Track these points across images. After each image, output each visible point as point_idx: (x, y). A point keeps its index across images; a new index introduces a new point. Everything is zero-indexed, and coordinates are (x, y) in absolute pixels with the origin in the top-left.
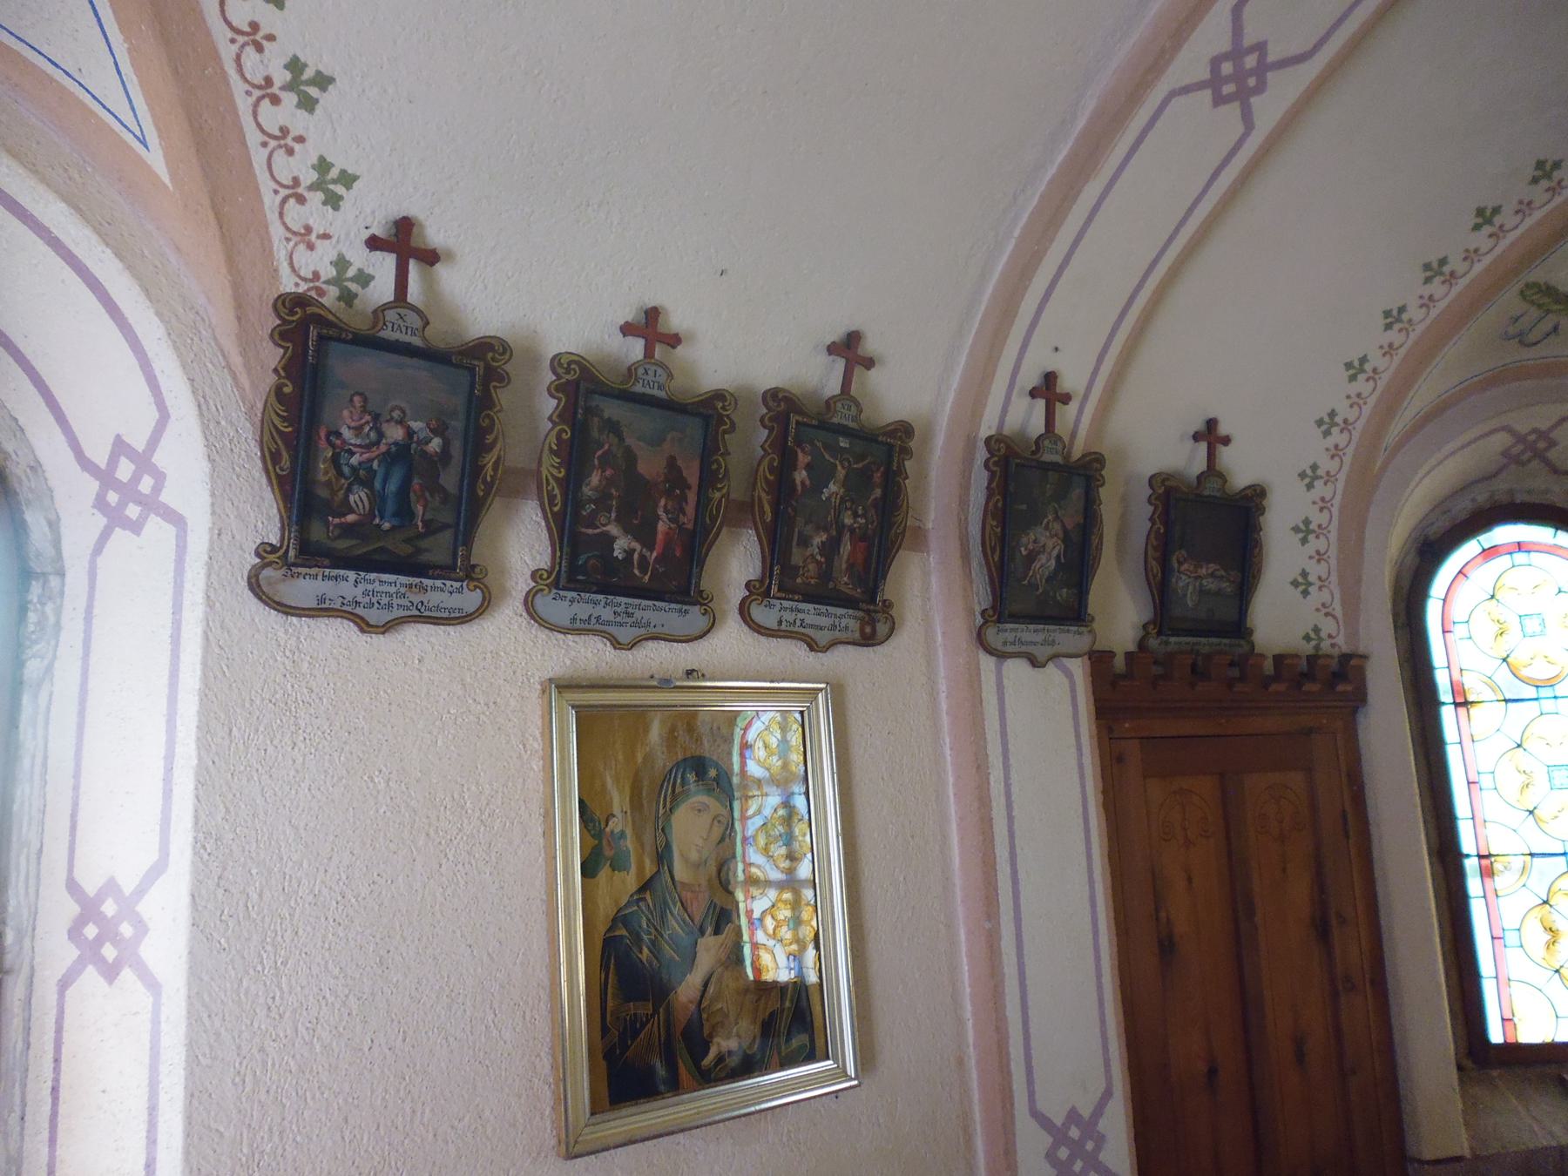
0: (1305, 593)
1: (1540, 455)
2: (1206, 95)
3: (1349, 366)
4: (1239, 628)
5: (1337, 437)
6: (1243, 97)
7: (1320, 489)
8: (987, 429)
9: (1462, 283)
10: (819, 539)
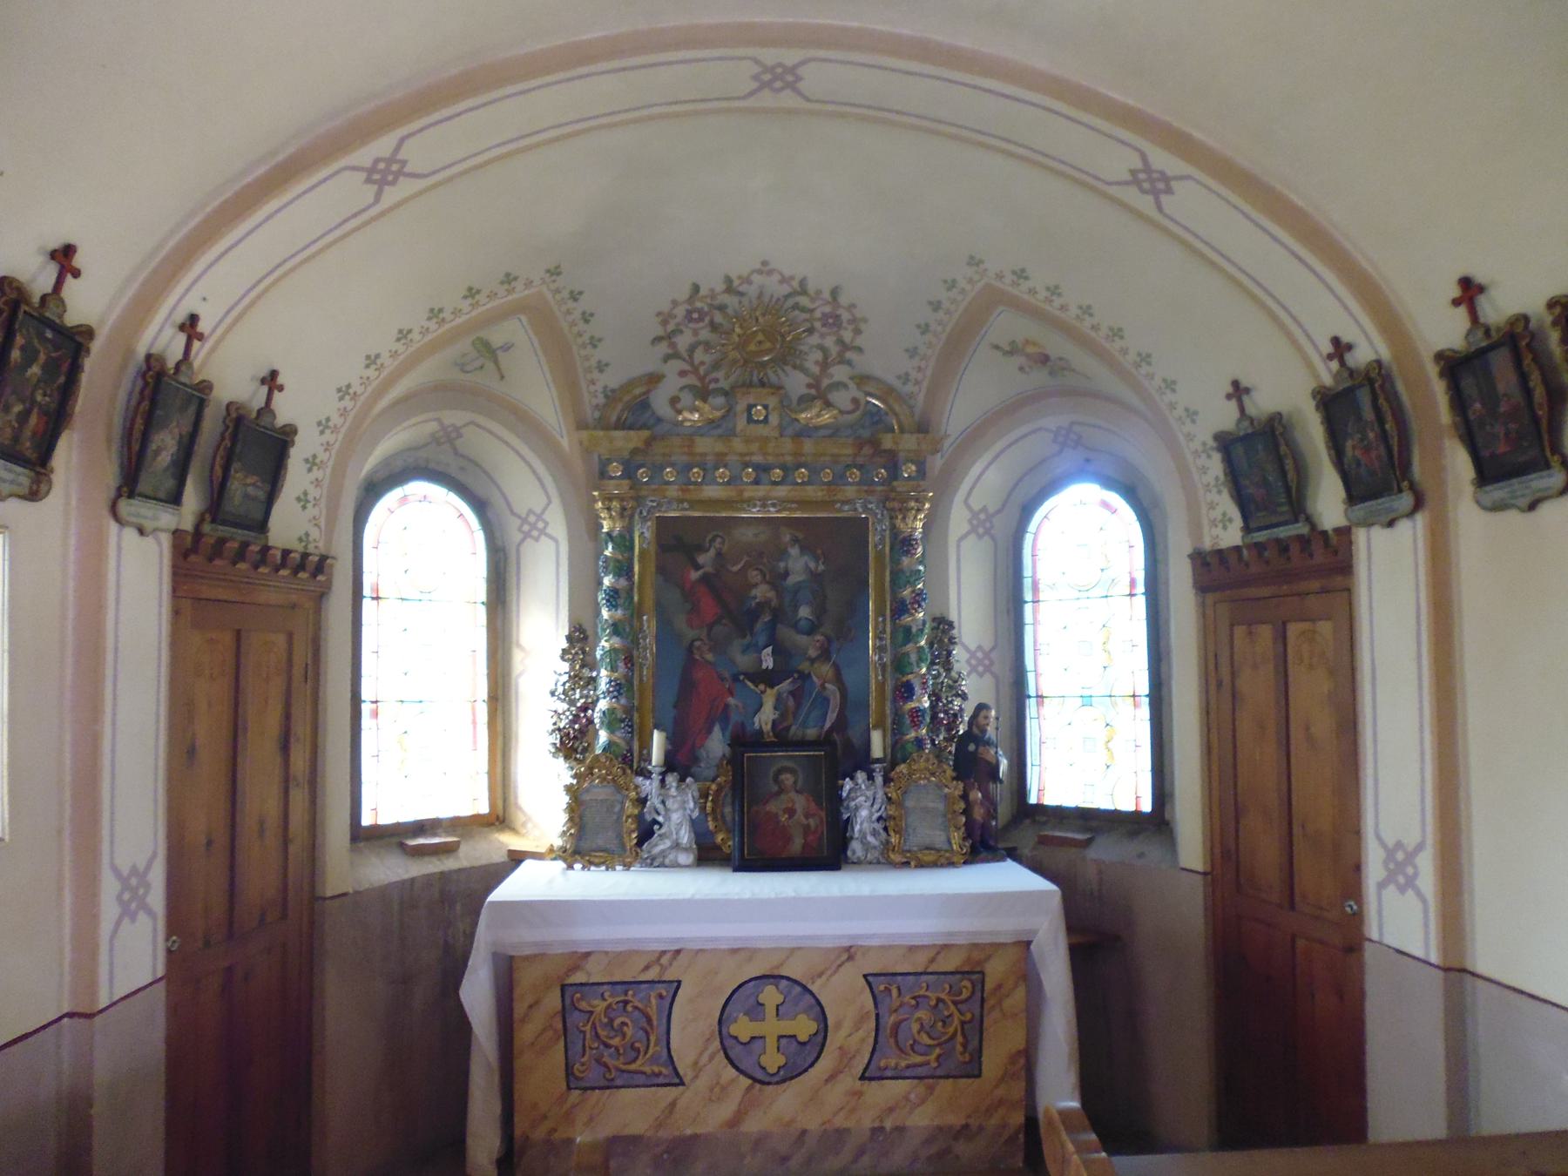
0: (304, 507)
1: (451, 441)
2: (364, 175)
3: (368, 357)
4: (262, 526)
5: (347, 403)
6: (382, 183)
7: (328, 436)
8: (141, 350)
9: (447, 326)
10: (18, 408)
